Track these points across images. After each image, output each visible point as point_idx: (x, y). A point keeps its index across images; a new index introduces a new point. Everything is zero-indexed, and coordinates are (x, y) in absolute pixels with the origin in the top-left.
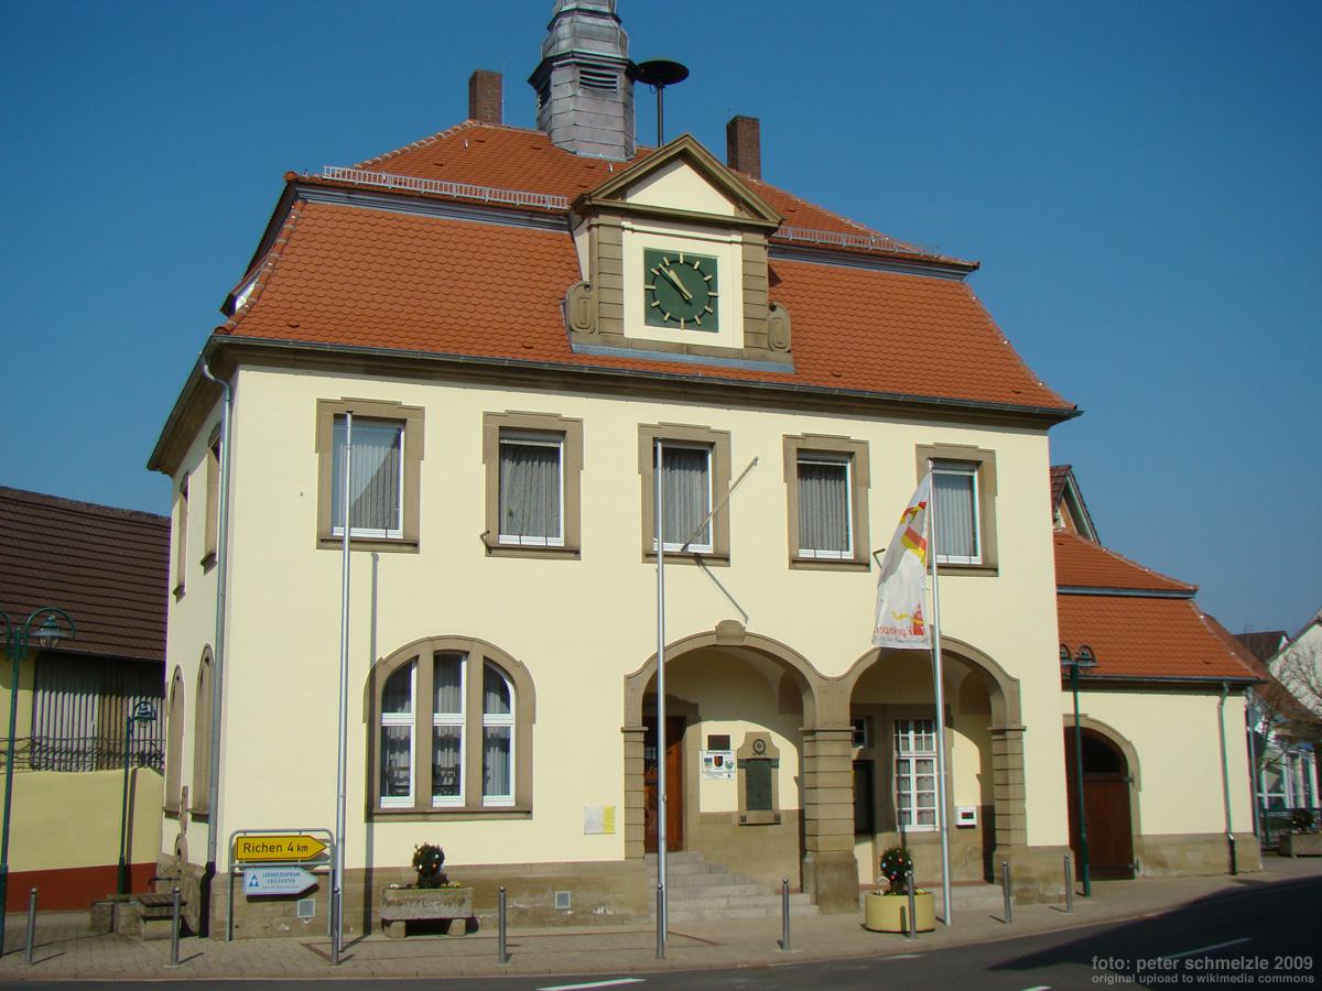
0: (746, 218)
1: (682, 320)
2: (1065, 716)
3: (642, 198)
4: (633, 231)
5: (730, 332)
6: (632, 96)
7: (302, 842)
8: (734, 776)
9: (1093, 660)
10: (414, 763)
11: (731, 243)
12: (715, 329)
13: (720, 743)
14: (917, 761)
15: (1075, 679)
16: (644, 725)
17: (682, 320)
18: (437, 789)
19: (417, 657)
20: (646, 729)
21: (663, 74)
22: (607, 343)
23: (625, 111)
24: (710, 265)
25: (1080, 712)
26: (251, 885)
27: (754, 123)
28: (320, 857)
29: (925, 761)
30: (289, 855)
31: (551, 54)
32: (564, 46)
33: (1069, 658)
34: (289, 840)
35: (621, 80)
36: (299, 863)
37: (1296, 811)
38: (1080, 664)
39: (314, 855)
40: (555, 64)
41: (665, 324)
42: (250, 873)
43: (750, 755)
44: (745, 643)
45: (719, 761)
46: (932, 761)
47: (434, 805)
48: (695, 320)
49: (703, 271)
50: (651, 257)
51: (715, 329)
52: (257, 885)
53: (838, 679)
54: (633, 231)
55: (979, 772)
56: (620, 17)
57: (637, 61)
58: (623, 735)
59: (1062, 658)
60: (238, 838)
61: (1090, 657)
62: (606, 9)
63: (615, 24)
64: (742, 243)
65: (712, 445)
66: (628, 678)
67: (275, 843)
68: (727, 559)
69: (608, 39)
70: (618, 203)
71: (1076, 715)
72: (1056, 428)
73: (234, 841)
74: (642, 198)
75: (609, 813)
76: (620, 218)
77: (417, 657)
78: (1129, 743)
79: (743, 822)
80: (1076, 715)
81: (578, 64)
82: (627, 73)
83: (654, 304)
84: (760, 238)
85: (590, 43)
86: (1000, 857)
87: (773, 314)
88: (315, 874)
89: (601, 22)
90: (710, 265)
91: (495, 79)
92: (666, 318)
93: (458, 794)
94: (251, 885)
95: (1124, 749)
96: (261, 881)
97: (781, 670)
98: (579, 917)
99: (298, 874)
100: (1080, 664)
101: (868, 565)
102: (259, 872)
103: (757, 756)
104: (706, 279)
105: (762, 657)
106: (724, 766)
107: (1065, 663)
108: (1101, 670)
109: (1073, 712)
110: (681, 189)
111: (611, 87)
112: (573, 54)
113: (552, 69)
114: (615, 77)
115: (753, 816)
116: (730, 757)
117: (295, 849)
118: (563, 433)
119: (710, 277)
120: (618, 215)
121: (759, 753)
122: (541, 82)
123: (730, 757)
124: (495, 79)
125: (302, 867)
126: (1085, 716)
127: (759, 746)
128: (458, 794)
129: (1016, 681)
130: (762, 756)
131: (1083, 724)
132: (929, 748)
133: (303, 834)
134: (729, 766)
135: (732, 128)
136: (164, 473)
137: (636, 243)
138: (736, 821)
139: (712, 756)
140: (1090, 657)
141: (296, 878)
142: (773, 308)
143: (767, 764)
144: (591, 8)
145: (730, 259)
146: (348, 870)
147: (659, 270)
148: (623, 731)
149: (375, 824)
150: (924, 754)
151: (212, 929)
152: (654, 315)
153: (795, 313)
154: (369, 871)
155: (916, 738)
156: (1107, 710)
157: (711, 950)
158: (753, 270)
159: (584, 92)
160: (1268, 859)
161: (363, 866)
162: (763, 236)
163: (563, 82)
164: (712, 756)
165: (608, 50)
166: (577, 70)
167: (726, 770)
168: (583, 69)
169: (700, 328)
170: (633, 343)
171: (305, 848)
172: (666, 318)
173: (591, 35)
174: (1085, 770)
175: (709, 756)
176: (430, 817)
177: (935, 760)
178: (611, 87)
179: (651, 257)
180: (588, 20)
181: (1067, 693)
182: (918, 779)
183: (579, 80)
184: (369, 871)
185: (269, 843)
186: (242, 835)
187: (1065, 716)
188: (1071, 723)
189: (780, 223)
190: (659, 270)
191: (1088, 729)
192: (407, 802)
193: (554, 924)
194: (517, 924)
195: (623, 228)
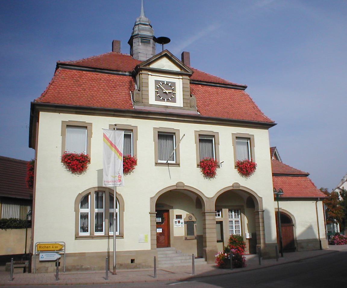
0: (183, 72)
1: (166, 99)
2: (275, 208)
3: (154, 66)
4: (152, 75)
5: (179, 102)
6: (155, 45)
7: (56, 245)
8: (183, 226)
9: (283, 192)
10: (91, 222)
11: (179, 79)
12: (155, 81)
13: (179, 217)
14: (235, 221)
15: (278, 198)
16: (156, 211)
17: (166, 99)
18: (97, 230)
19: (90, 193)
20: (157, 212)
21: (164, 40)
22: (145, 105)
23: (153, 49)
24: (174, 84)
25: (279, 207)
26: (41, 258)
27: (188, 53)
28: (61, 250)
29: (237, 221)
30: (53, 249)
31: (133, 35)
32: (136, 33)
33: (276, 191)
34: (52, 245)
35: (152, 41)
36: (56, 251)
37: (336, 233)
38: (279, 193)
39: (59, 248)
40: (134, 37)
41: (161, 100)
42: (41, 254)
43: (188, 220)
44: (185, 188)
45: (179, 222)
46: (239, 221)
47: (95, 235)
48: (169, 99)
49: (172, 86)
50: (157, 82)
51: (155, 81)
52: (43, 258)
53: (211, 198)
54: (152, 75)
55: (247, 223)
56: (152, 26)
57: (157, 37)
58: (150, 214)
59: (274, 192)
60: (38, 244)
61: (282, 191)
62: (148, 24)
63: (150, 27)
64: (182, 79)
65: (175, 133)
66: (151, 198)
67: (48, 246)
68: (179, 165)
69: (148, 31)
70: (147, 67)
71: (278, 208)
72: (272, 129)
73: (37, 244)
74: (154, 66)
75: (146, 237)
76: (148, 72)
77: (90, 193)
78: (293, 215)
79: (186, 239)
80: (278, 208)
81: (140, 37)
82: (153, 39)
83: (158, 95)
84: (187, 77)
85: (143, 32)
86: (258, 247)
87: (191, 98)
88: (60, 254)
89: (146, 27)
90: (174, 84)
91: (119, 42)
92: (161, 99)
93: (103, 231)
94: (41, 258)
95: (292, 217)
96: (44, 257)
97: (196, 197)
98: (137, 266)
99: (55, 255)
100: (279, 193)
101: (219, 166)
102: (44, 254)
103: (190, 220)
104: (172, 88)
105: (192, 193)
106: (180, 223)
107: (275, 193)
108: (285, 195)
109: (277, 207)
110: (164, 64)
111: (149, 43)
112: (138, 34)
113: (133, 38)
114: (150, 40)
115: (189, 237)
116: (182, 221)
117: (54, 247)
118: (132, 130)
119: (173, 88)
120: (147, 71)
121: (190, 220)
122: (131, 43)
123: (182, 221)
124: (119, 42)
125: (57, 253)
126: (281, 208)
127: (190, 218)
128: (103, 231)
129: (261, 198)
130: (191, 220)
131: (280, 210)
132: (238, 217)
133: (57, 243)
134: (182, 223)
135: (183, 54)
136: (33, 148)
137: (152, 80)
138: (184, 238)
139: (177, 221)
140: (282, 191)
141: (55, 256)
142: (191, 96)
143: (193, 222)
144: (144, 23)
145: (179, 83)
146: (118, 252)
147: (159, 86)
148: (150, 213)
149: (110, 240)
150: (237, 219)
151: (32, 271)
152: (158, 98)
153: (197, 99)
154: (108, 252)
155: (235, 215)
156: (287, 207)
157: (172, 275)
158: (185, 86)
159: (142, 44)
160: (329, 245)
161: (106, 251)
162: (188, 77)
163: (137, 43)
164: (177, 221)
165: (148, 33)
166: (140, 39)
167: (181, 224)
168: (141, 38)
169: (170, 101)
170: (151, 105)
171: (57, 247)
172: (161, 99)
173: (144, 30)
174: (281, 223)
175: (176, 221)
176: (94, 238)
177: (240, 221)
178: (149, 43)
179: (157, 82)
180: (143, 26)
181: (276, 202)
182: (235, 226)
183: (140, 41)
184: (108, 252)
185: (46, 246)
186: (39, 243)
187: (275, 208)
188: (277, 210)
189: (193, 73)
190: (159, 86)
191: (282, 212)
192: (87, 234)
193: (130, 268)
194: (119, 268)
195: (149, 74)
